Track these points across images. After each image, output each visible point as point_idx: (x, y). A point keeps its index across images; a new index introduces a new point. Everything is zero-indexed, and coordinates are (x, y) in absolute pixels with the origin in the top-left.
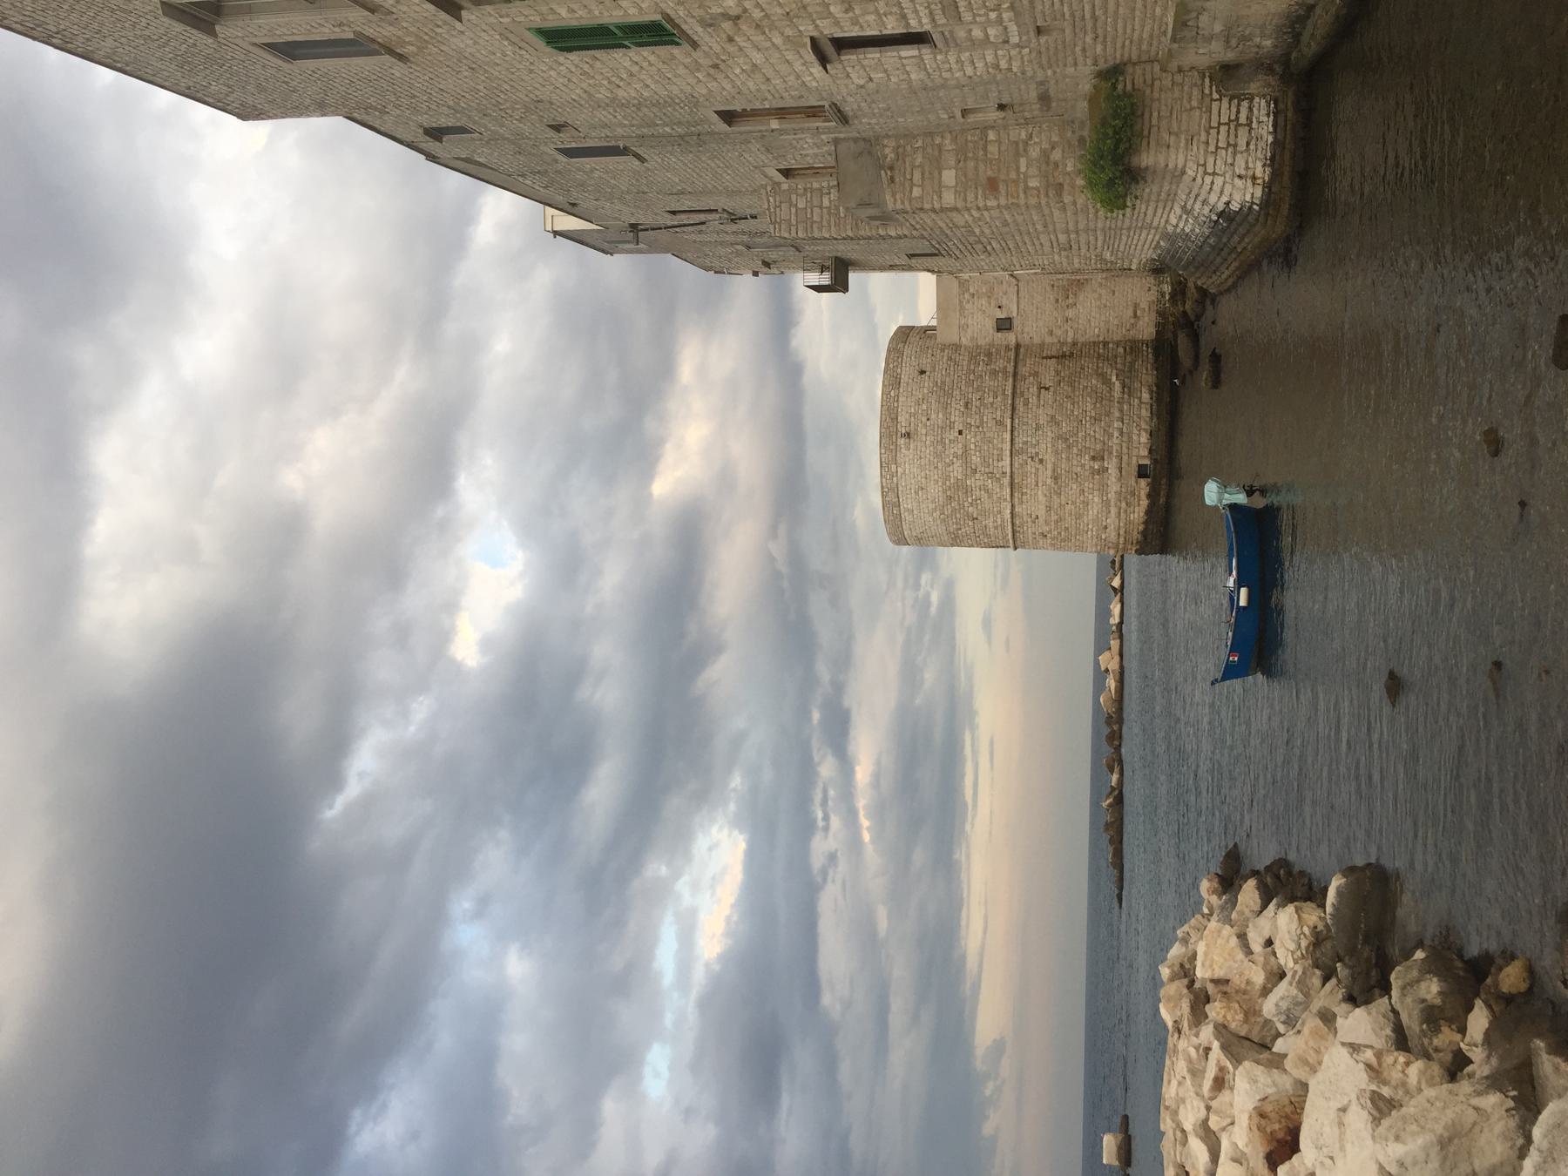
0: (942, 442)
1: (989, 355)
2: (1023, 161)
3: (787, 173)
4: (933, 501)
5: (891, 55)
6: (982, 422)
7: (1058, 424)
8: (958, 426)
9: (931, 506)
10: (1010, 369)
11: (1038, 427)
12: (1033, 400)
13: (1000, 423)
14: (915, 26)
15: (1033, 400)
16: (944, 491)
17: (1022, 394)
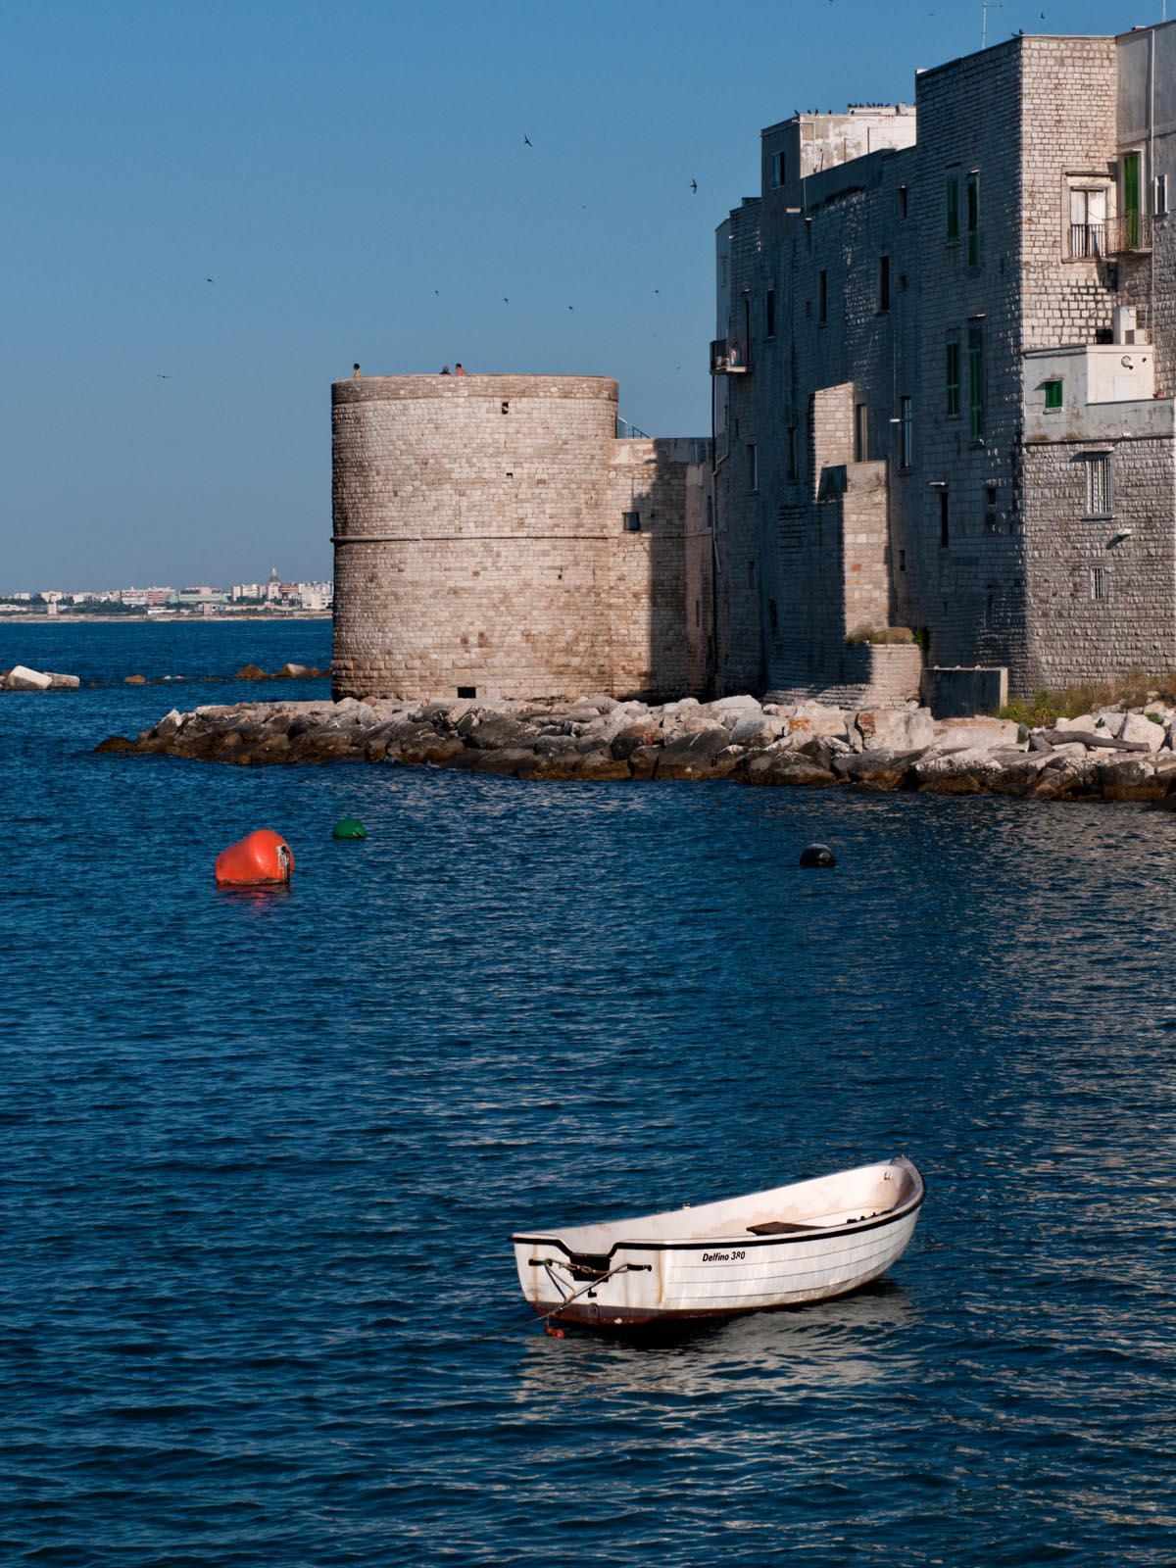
0: (498, 453)
1: (597, 505)
2: (870, 587)
3: (823, 274)
4: (419, 441)
5: (937, 521)
6: (522, 501)
7: (521, 591)
8: (517, 472)
9: (413, 439)
10: (582, 532)
11: (517, 569)
12: (547, 561)
13: (521, 524)
14: (951, 541)
15: (547, 561)
16: (434, 455)
17: (554, 548)
